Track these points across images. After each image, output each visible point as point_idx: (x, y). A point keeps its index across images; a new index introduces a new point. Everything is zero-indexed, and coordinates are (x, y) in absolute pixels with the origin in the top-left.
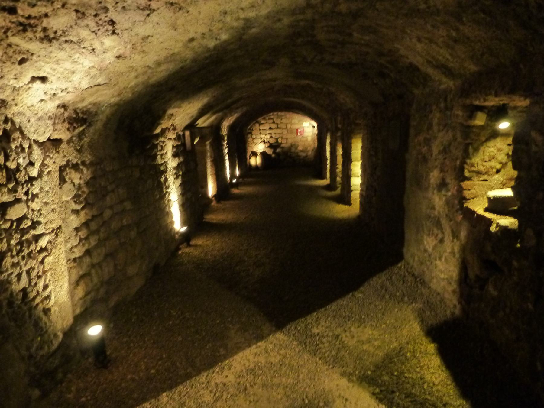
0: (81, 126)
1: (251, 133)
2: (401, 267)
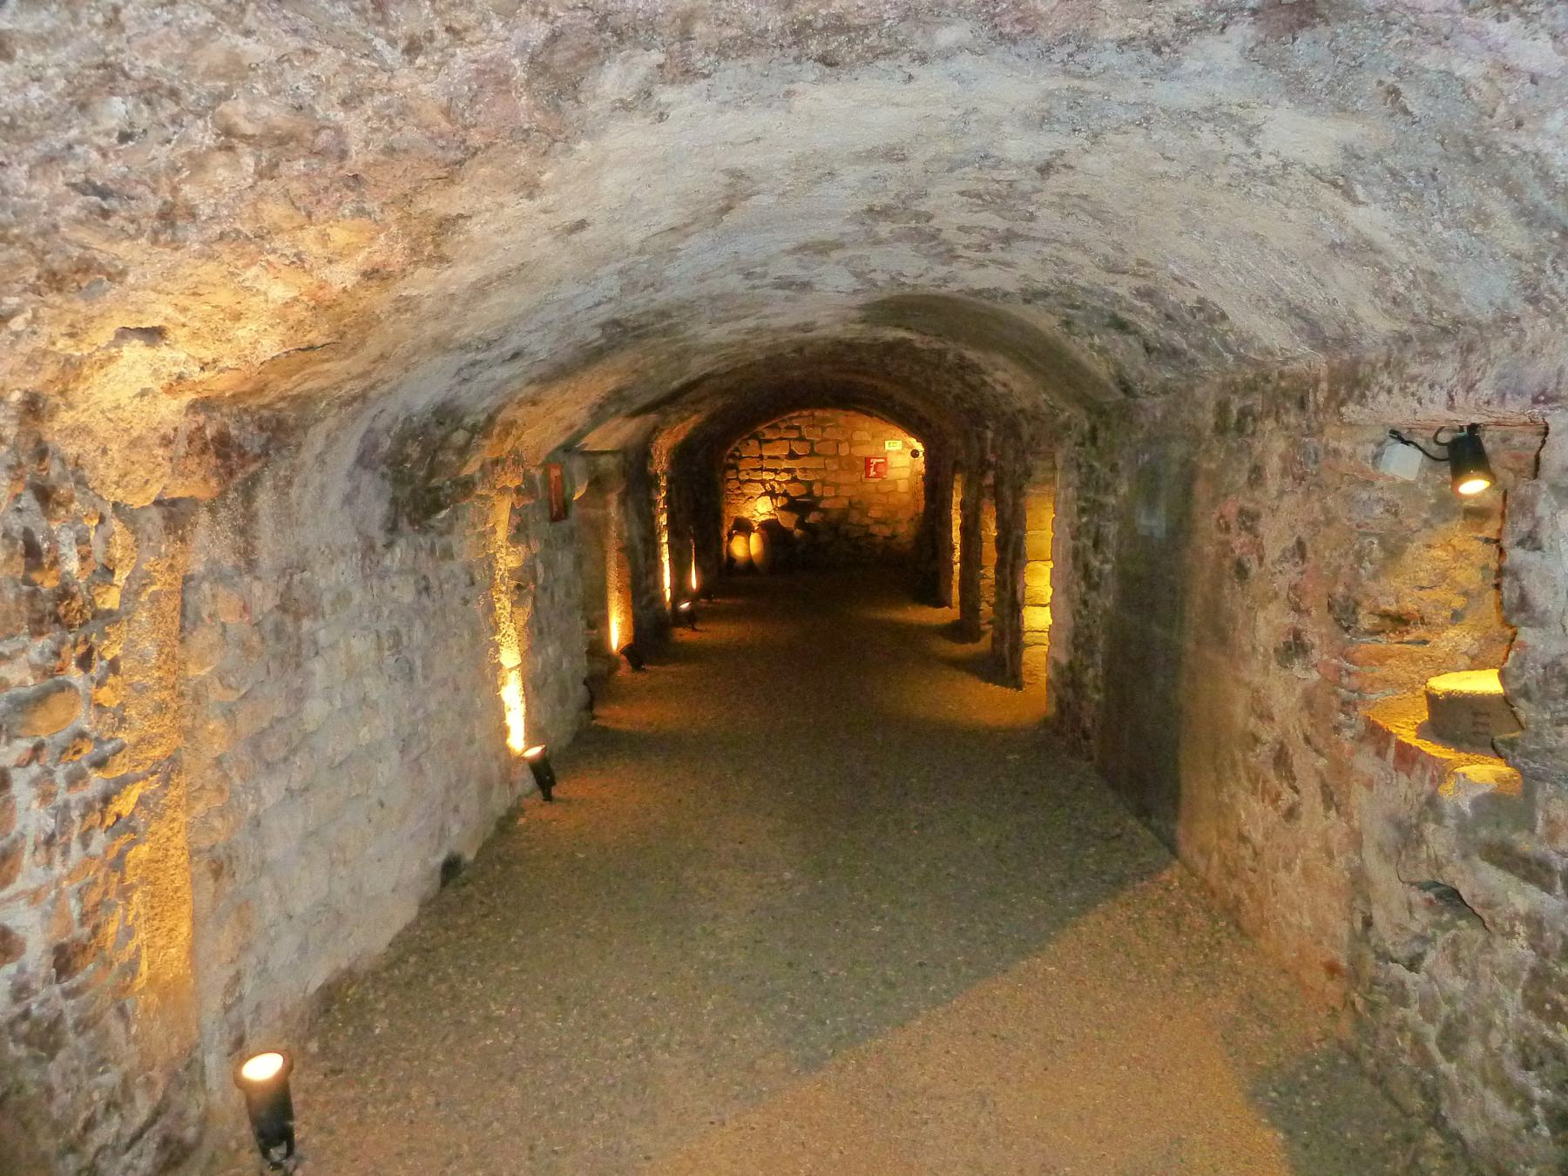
2: (1171, 883)
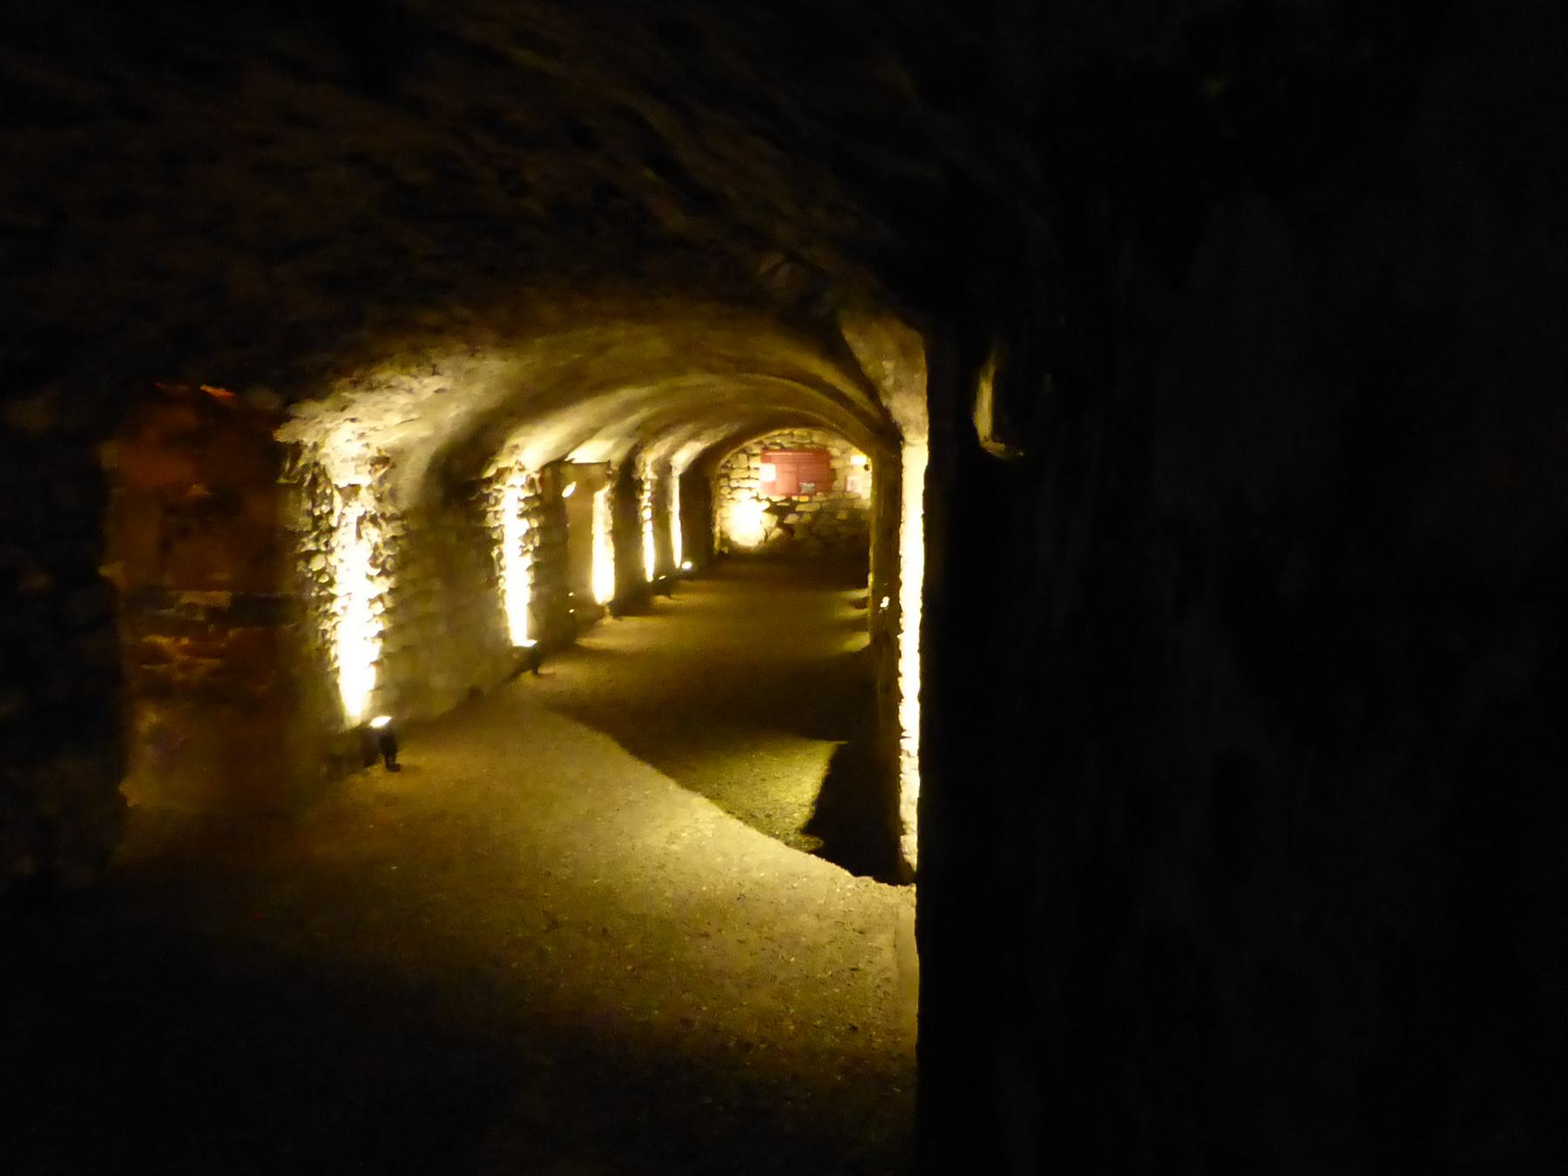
0: (383, 467)
1: (727, 476)
